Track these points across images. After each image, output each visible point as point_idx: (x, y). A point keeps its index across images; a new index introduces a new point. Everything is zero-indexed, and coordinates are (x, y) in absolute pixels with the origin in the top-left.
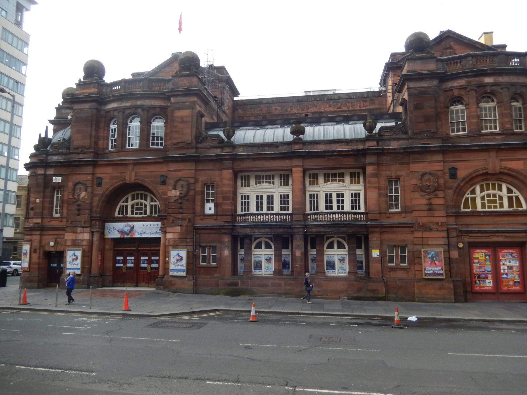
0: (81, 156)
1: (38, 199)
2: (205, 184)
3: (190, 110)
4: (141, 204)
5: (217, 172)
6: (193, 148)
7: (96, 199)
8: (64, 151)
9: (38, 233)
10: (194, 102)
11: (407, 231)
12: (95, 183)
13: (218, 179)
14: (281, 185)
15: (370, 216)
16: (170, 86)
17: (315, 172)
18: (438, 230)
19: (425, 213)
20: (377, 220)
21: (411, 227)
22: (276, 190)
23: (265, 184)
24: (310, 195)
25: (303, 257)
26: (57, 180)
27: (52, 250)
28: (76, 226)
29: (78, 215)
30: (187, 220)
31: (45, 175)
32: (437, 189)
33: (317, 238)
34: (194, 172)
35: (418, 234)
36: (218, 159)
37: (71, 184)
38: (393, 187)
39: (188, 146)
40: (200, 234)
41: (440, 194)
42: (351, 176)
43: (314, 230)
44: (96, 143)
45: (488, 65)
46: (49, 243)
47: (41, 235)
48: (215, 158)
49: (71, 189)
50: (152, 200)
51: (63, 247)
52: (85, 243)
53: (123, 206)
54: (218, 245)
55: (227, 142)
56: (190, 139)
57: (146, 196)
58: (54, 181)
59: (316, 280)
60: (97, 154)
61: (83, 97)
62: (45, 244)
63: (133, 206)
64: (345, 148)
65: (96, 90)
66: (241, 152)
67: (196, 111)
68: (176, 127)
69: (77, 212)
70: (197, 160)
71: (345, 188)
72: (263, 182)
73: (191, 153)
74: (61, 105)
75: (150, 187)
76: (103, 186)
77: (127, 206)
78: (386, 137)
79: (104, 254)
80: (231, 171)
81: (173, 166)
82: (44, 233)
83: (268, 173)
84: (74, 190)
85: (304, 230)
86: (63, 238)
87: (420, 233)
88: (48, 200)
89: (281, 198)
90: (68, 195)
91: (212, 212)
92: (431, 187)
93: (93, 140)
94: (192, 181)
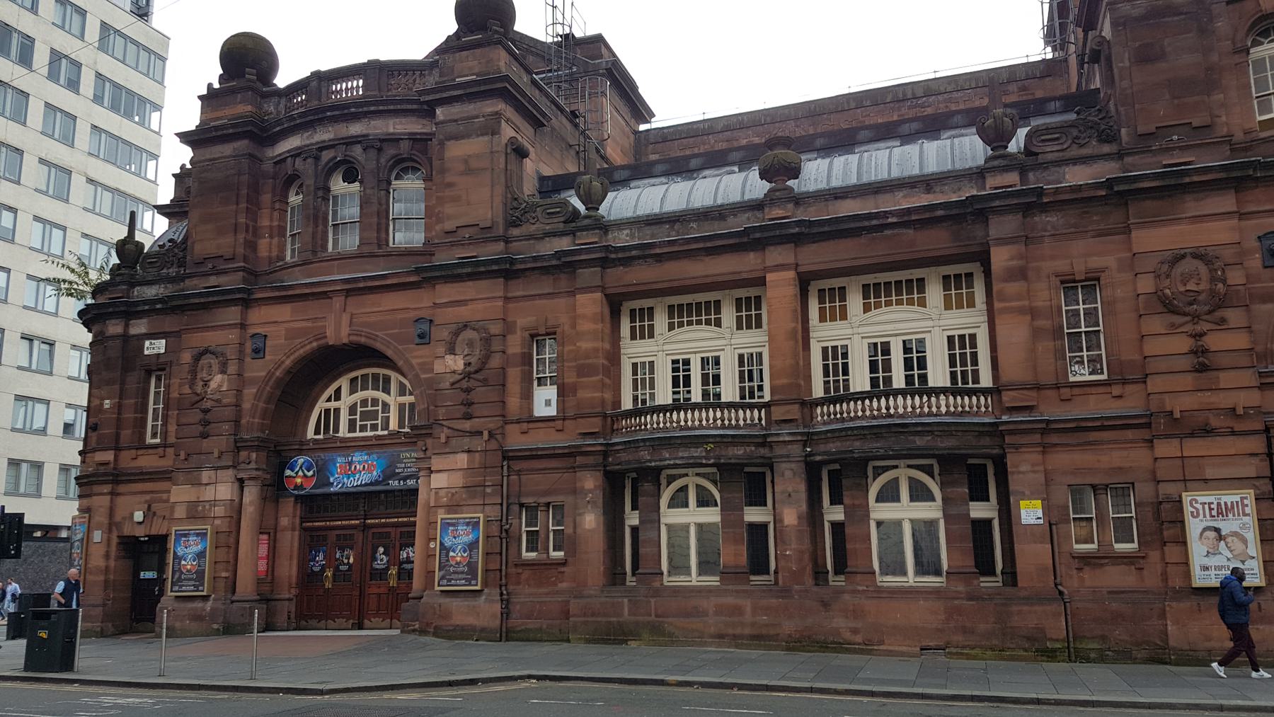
0: (213, 280)
1: (107, 401)
2: (532, 336)
3: (486, 138)
4: (375, 402)
5: (562, 302)
6: (496, 239)
7: (250, 392)
8: (173, 271)
9: (106, 488)
10: (498, 115)
11: (1132, 442)
12: (249, 347)
13: (564, 319)
14: (739, 327)
15: (1008, 398)
16: (431, 80)
17: (836, 283)
18: (1233, 433)
19: (1188, 380)
20: (1029, 408)
21: (1146, 426)
22: (724, 344)
23: (695, 327)
24: (825, 350)
25: (805, 528)
26: (155, 347)
27: (140, 532)
29: (204, 436)
30: (486, 434)
31: (125, 337)
32: (1220, 302)
33: (842, 469)
34: (501, 303)
35: (1166, 448)
36: (565, 265)
37: (187, 357)
38: (1081, 307)
39: (485, 234)
40: (519, 473)
41: (1234, 316)
42: (946, 287)
43: (833, 447)
44: (252, 246)
46: (132, 515)
47: (113, 494)
48: (554, 262)
49: (186, 368)
50: (402, 392)
51: (166, 522)
52: (219, 511)
53: (327, 411)
54: (568, 500)
55: (586, 217)
56: (490, 216)
57: (387, 380)
58: (146, 352)
59: (847, 597)
60: (252, 275)
62: (124, 518)
63: (352, 410)
64: (922, 199)
65: (249, 108)
66: (622, 238)
67: (504, 140)
68: (450, 185)
69: (201, 428)
70: (507, 271)
71: (930, 323)
72: (690, 323)
73: (492, 251)
74: (189, 166)
75: (389, 353)
76: (267, 357)
77: (337, 411)
78: (1050, 157)
79: (275, 541)
80: (598, 295)
81: (447, 292)
82: (122, 488)
84: (194, 372)
85: (805, 446)
86: (167, 501)
87: (1176, 442)
88: (132, 401)
89: (741, 363)
90: (181, 385)
91: (552, 411)
92: (1201, 298)
93: (241, 237)
94: (495, 329)
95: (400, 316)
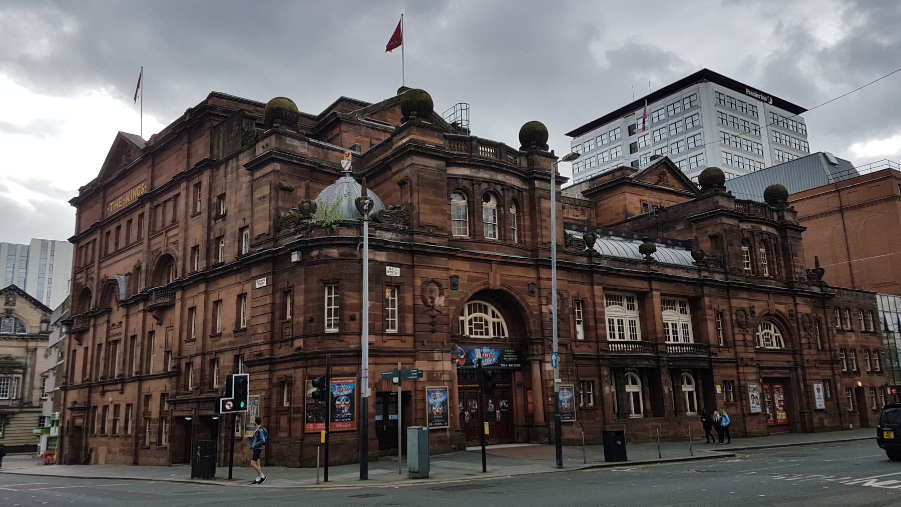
0: (431, 239)
4: (481, 319)
9: (267, 367)
26: (394, 272)
28: (432, 351)
29: (433, 331)
45: (460, 151)
57: (486, 307)
61: (428, 149)
63: (470, 322)
83: (617, 293)
95: (521, 280)
